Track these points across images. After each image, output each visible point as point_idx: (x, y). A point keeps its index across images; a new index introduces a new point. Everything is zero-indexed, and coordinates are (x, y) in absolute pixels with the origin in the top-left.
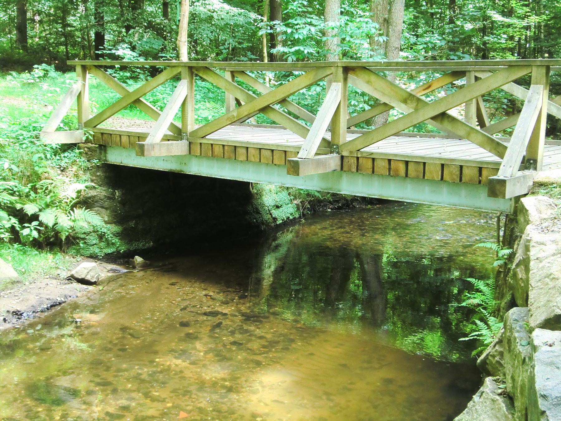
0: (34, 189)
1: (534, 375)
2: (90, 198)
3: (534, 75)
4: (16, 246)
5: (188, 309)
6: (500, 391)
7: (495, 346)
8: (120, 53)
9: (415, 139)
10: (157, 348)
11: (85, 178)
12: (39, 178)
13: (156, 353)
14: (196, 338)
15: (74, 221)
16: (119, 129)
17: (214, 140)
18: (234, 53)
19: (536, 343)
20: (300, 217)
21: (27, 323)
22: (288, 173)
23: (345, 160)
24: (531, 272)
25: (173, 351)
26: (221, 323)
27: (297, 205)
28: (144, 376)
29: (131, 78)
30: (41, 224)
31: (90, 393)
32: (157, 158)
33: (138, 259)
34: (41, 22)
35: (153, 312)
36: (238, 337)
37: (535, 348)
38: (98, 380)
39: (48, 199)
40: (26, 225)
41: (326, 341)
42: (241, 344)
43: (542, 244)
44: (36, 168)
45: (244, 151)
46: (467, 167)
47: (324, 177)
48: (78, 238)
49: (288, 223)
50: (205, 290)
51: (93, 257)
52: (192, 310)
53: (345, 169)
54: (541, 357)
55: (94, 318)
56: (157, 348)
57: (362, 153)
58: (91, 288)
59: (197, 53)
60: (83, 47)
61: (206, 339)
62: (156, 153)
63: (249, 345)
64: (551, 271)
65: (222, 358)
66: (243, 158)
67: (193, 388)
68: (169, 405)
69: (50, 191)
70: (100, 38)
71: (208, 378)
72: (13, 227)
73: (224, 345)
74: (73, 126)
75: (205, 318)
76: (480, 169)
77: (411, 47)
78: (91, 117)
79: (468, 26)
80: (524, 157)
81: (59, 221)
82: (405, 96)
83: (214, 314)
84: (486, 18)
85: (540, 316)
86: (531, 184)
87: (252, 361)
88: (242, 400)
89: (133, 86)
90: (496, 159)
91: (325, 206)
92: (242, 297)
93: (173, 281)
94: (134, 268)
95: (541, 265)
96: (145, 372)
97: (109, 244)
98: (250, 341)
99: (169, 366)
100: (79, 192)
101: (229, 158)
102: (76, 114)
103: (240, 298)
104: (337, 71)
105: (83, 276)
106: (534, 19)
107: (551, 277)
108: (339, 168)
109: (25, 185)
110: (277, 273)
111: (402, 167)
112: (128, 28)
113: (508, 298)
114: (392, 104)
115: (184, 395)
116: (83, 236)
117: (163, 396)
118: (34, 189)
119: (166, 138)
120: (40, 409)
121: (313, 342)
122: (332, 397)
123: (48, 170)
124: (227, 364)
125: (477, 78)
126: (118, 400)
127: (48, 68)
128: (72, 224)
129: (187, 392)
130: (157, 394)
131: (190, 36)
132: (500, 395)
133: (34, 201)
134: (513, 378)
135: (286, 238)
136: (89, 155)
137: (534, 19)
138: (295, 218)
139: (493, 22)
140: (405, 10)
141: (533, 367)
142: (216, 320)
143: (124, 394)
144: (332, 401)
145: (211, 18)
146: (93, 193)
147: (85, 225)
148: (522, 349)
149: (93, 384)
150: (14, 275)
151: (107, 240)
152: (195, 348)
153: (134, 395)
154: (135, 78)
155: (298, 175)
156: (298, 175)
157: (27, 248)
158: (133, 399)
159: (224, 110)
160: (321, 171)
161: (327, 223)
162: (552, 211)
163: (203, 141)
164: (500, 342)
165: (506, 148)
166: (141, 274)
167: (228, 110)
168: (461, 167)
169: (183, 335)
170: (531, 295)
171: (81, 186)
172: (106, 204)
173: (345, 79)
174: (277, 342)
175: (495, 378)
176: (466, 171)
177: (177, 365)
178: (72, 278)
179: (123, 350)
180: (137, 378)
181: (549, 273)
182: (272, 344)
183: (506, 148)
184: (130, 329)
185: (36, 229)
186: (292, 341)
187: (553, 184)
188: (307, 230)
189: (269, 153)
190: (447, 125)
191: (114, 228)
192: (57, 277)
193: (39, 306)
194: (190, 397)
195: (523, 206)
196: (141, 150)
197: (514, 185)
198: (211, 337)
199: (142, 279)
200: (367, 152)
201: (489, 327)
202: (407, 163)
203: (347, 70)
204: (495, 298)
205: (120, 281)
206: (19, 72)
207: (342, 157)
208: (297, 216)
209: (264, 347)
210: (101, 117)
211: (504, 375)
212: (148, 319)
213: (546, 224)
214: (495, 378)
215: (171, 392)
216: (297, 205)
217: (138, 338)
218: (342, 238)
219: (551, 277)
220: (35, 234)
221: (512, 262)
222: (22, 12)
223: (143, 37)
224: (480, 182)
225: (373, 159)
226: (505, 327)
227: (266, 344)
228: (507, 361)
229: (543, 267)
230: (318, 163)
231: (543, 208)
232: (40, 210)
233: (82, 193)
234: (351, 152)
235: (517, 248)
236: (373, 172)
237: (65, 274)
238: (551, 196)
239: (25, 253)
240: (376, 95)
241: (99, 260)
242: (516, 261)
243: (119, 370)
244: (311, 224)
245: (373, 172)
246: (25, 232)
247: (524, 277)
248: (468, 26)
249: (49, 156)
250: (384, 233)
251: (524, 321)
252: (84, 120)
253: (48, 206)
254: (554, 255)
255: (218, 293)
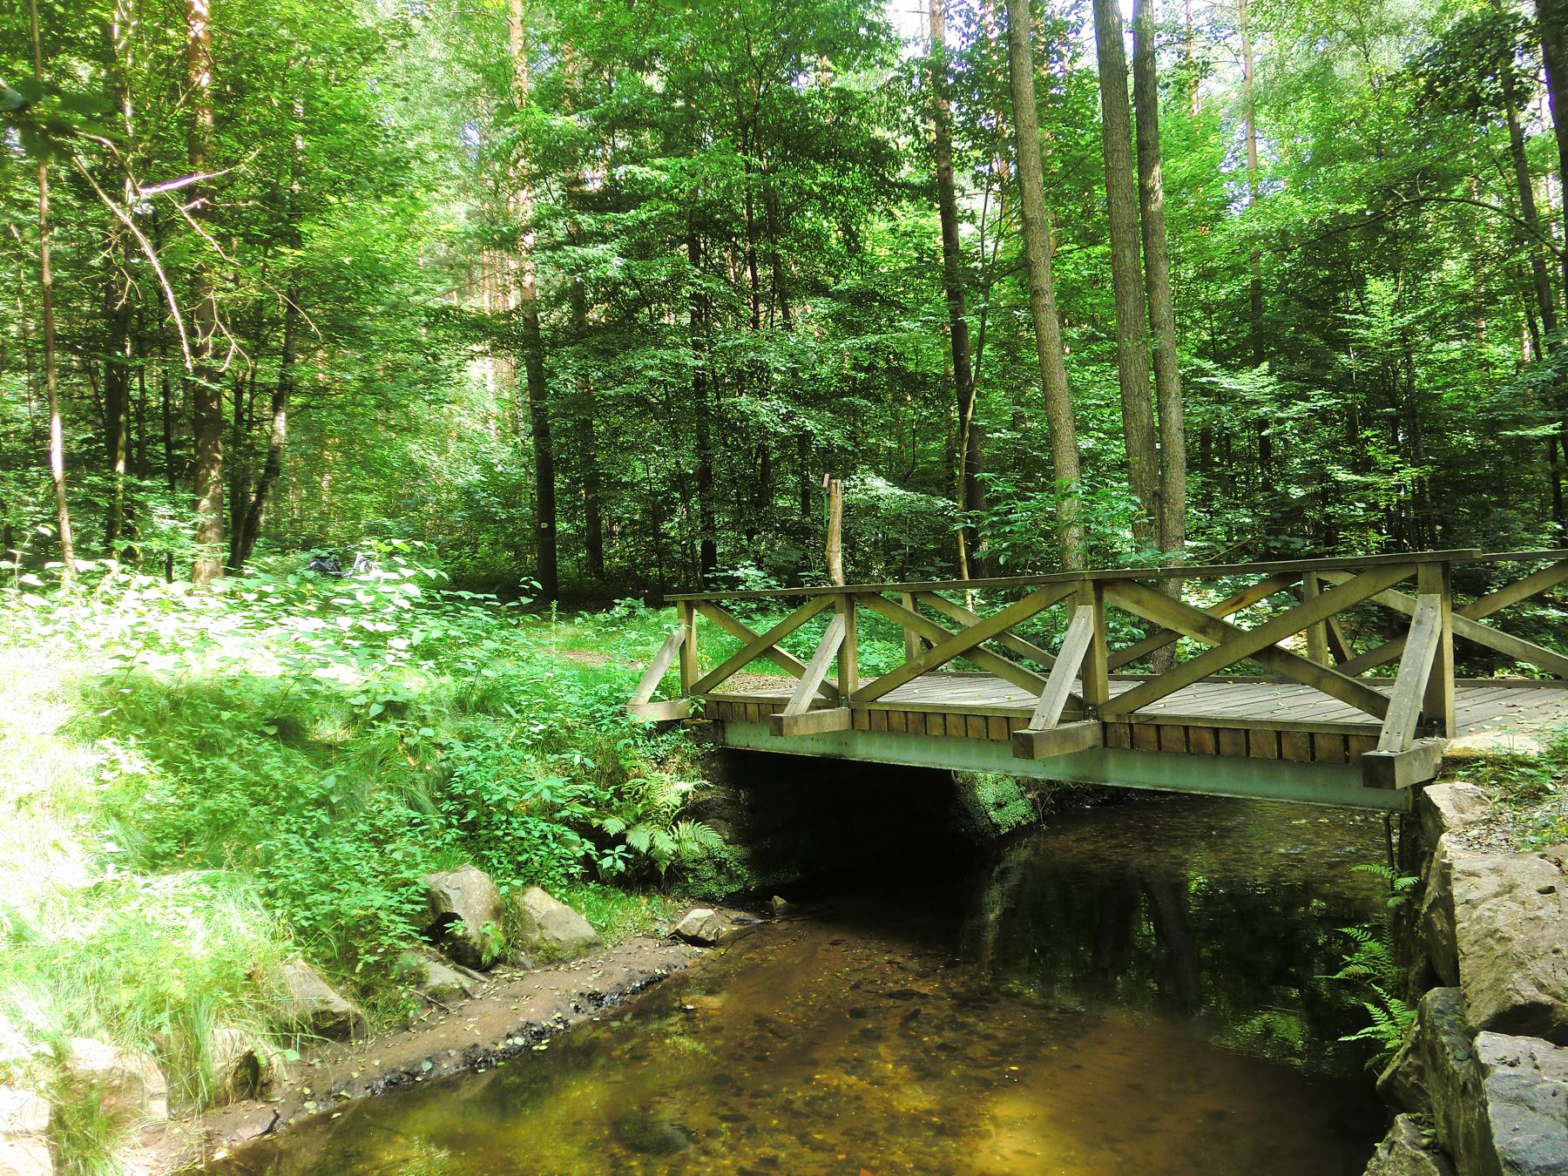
0: (618, 794)
1: (1488, 1122)
2: (701, 804)
3: (1421, 578)
4: (592, 885)
5: (864, 987)
6: (1425, 1141)
7: (1406, 1056)
8: (740, 573)
9: (1225, 686)
10: (816, 1055)
11: (693, 772)
12: (626, 777)
13: (815, 1064)
14: (879, 1038)
15: (678, 842)
16: (743, 693)
17: (890, 704)
18: (915, 558)
19: (1484, 1058)
20: (1039, 821)
21: (611, 1012)
22: (1016, 755)
23: (1110, 730)
24: (1459, 926)
25: (841, 1060)
26: (918, 1012)
27: (1033, 800)
28: (797, 1106)
29: (758, 610)
30: (629, 849)
31: (712, 1133)
32: (802, 738)
33: (779, 901)
34: (622, 535)
35: (806, 992)
36: (949, 1035)
37: (1483, 1070)
38: (723, 1111)
39: (639, 810)
40: (607, 851)
41: (1101, 1043)
42: (955, 1049)
43: (1473, 874)
44: (622, 762)
45: (940, 720)
46: (1323, 735)
47: (1076, 758)
48: (685, 869)
49: (1019, 832)
50: (888, 952)
51: (707, 900)
52: (869, 988)
53: (1110, 743)
54: (1496, 1086)
55: (713, 1002)
56: (816, 1055)
57: (1138, 716)
58: (706, 951)
59: (856, 564)
60: (685, 567)
61: (895, 1040)
62: (800, 730)
63: (970, 1051)
64: (1496, 926)
65: (924, 1073)
66: (938, 731)
67: (878, 1128)
68: (841, 1157)
69: (642, 797)
70: (709, 548)
71: (903, 1110)
72: (587, 855)
73: (927, 1051)
74: (674, 693)
75: (891, 1002)
76: (1346, 739)
77: (1200, 531)
78: (701, 676)
79: (1297, 492)
80: (1421, 715)
81: (657, 842)
82: (1201, 621)
83: (906, 995)
84: (1325, 477)
85: (1483, 1009)
86: (1439, 761)
87: (975, 1078)
88: (964, 1150)
89: (763, 626)
90: (1368, 719)
91: (1081, 800)
92: (951, 965)
93: (836, 937)
94: (773, 916)
95: (1475, 914)
96: (800, 1095)
97: (733, 877)
98: (969, 1043)
99: (838, 1087)
100: (685, 795)
101: (917, 732)
102: (677, 673)
103: (947, 966)
104: (1083, 589)
105: (694, 933)
106: (1409, 474)
107: (1498, 935)
108: (1100, 743)
109: (605, 789)
110: (1008, 914)
111: (1208, 738)
112: (750, 534)
113: (1420, 964)
114: (1181, 631)
115: (864, 1141)
116: (691, 866)
117: (832, 1141)
118: (618, 794)
119: (816, 705)
120: (634, 1163)
121: (1079, 1044)
122: (1119, 1146)
123: (639, 762)
124: (934, 1085)
125: (1322, 583)
126: (758, 1147)
127: (635, 603)
128: (675, 847)
129: (870, 1135)
130: (819, 1137)
131: (846, 537)
132: (1425, 1148)
133: (618, 813)
134: (1447, 1118)
135: (1020, 855)
136: (698, 736)
137: (1409, 474)
138: (1030, 823)
139: (1337, 483)
140: (1188, 474)
141: (1484, 1104)
142: (912, 1005)
143: (766, 1137)
144: (1119, 1152)
145: (875, 508)
146: (707, 796)
147: (696, 847)
148: (1456, 1065)
149: (714, 1119)
150: (589, 932)
151: (729, 870)
152: (878, 1057)
153: (782, 1138)
154: (764, 610)
155: (1032, 757)
156: (1032, 757)
157: (608, 888)
158: (781, 1146)
159: (902, 651)
160: (1070, 749)
161: (1087, 830)
162: (1482, 808)
163: (874, 707)
164: (1415, 1049)
165: (1387, 701)
166: (784, 925)
167: (909, 652)
168: (1312, 735)
169: (856, 1032)
170: (1465, 968)
171: (687, 786)
172: (726, 814)
173: (1099, 600)
174: (1017, 1045)
175: (1413, 1116)
176: (1321, 743)
177: (850, 1086)
178: (677, 937)
179: (763, 1059)
180: (787, 1108)
181: (1492, 928)
182: (1005, 1051)
183: (1387, 701)
184: (771, 1021)
185: (621, 858)
186: (1041, 1043)
187: (1478, 759)
188: (1052, 843)
189: (981, 722)
190: (1278, 666)
191: (739, 851)
192: (655, 935)
193: (629, 983)
194: (875, 1144)
195: (1429, 800)
196: (778, 727)
197: (1410, 764)
198: (903, 1035)
199: (785, 933)
200: (1146, 715)
201: (1391, 1017)
202: (1216, 731)
203: (1100, 585)
204: (1395, 964)
205: (752, 939)
206: (593, 613)
207: (1105, 726)
208: (1034, 819)
209: (993, 1053)
210: (716, 677)
211: (1430, 1110)
212: (798, 1004)
213: (1475, 832)
214: (1413, 1116)
215: (843, 1134)
216: (1033, 800)
217: (784, 1038)
218: (1114, 857)
219: (1498, 935)
220: (620, 865)
221: (1421, 900)
222: (594, 521)
223: (773, 545)
224: (1347, 759)
225: (1158, 727)
226: (1421, 1021)
227: (995, 1048)
228: (1431, 1083)
229: (1480, 918)
230: (1065, 737)
231: (1465, 803)
232: (628, 827)
233: (690, 797)
234: (1119, 716)
235: (1427, 874)
236: (1160, 747)
237: (665, 930)
238: (1478, 782)
239: (605, 896)
240: (1154, 619)
241: (718, 903)
242: (1429, 900)
243: (756, 1095)
244: (1058, 833)
245: (1160, 747)
246: (606, 863)
247: (1446, 928)
248: (1297, 492)
249: (640, 742)
250: (1186, 843)
251: (1455, 1012)
252: (691, 683)
253: (638, 819)
254: (1497, 895)
255: (911, 958)
